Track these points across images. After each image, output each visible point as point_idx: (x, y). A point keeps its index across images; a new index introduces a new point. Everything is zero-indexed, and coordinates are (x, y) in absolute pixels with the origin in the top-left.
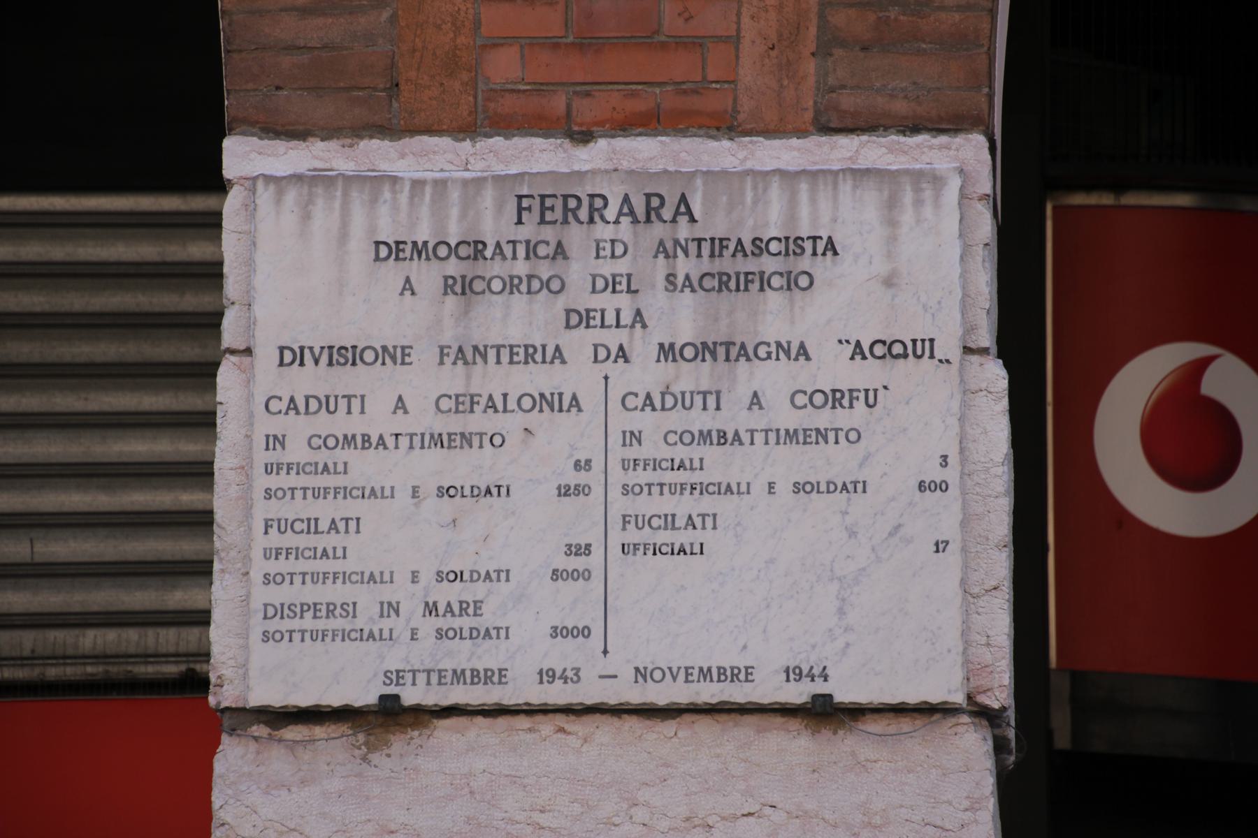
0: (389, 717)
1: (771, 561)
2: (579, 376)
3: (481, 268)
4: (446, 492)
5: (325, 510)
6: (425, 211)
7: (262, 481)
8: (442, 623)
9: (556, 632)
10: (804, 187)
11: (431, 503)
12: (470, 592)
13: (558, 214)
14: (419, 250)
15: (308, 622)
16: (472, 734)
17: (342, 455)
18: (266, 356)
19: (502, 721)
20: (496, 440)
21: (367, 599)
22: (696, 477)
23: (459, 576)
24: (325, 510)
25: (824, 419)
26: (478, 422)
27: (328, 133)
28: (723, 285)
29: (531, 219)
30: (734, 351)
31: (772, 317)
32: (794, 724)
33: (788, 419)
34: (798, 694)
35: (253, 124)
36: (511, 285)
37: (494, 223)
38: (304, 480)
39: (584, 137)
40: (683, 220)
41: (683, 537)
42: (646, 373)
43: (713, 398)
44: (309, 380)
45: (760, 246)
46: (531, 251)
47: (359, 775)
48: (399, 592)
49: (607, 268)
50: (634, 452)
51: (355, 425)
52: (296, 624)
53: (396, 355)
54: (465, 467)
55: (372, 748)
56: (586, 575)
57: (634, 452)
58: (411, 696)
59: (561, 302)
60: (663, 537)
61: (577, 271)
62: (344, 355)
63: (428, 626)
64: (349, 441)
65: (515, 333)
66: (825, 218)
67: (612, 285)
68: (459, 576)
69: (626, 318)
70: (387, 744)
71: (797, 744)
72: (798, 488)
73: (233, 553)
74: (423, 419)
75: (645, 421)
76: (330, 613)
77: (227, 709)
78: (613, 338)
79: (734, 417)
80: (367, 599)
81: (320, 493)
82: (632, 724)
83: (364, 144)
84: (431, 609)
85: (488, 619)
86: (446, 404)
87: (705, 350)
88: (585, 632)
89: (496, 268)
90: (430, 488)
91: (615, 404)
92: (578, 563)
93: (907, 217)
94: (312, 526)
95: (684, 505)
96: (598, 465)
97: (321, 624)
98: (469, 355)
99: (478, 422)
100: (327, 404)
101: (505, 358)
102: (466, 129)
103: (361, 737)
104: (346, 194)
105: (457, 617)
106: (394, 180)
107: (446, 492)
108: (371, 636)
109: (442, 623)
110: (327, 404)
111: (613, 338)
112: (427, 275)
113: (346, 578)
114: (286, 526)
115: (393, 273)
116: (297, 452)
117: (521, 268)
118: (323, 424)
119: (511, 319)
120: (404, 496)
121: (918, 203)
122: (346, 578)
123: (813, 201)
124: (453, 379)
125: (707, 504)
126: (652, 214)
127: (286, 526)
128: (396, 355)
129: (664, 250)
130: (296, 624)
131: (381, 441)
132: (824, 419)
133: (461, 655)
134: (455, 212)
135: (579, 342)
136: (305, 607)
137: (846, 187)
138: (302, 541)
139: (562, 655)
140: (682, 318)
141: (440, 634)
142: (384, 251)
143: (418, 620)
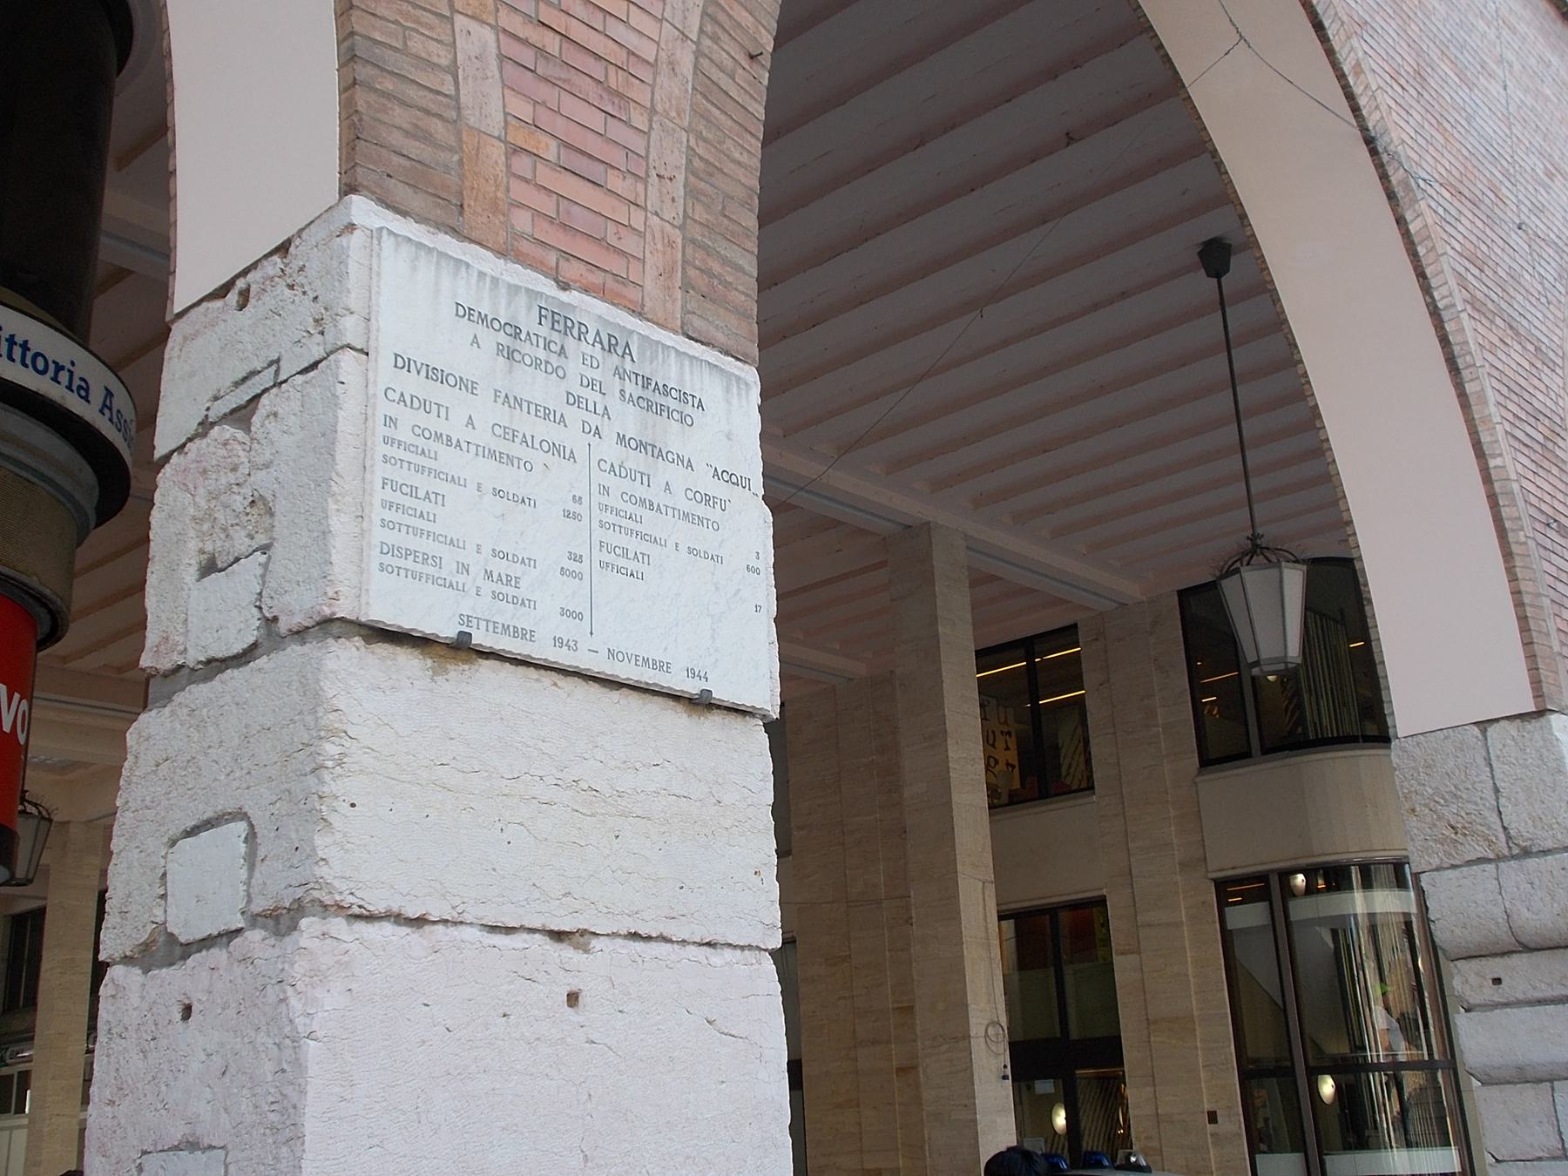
0: (462, 649)
1: (678, 595)
2: (571, 437)
3: (517, 345)
4: (497, 492)
5: (424, 483)
6: (486, 294)
7: (383, 449)
8: (499, 588)
9: (563, 612)
10: (687, 362)
11: (489, 498)
12: (517, 570)
13: (561, 328)
14: (483, 319)
15: (409, 563)
16: (503, 675)
17: (433, 445)
18: (384, 361)
19: (521, 669)
20: (528, 466)
21: (449, 556)
22: (638, 527)
23: (506, 556)
24: (424, 483)
25: (701, 510)
26: (516, 449)
27: (421, 220)
28: (649, 408)
29: (546, 323)
30: (656, 452)
31: (672, 436)
32: (679, 707)
33: (685, 506)
34: (692, 687)
35: (373, 193)
36: (536, 363)
37: (528, 322)
38: (407, 456)
39: (564, 286)
40: (628, 358)
41: (633, 566)
42: (609, 450)
43: (645, 478)
44: (413, 384)
45: (666, 391)
46: (547, 347)
47: (431, 690)
48: (468, 557)
49: (590, 374)
50: (605, 500)
51: (441, 426)
52: (401, 563)
53: (470, 387)
54: (509, 479)
55: (435, 673)
56: (579, 576)
57: (605, 500)
58: (480, 638)
59: (564, 386)
60: (621, 562)
61: (574, 367)
62: (436, 375)
63: (488, 587)
64: (439, 436)
65: (538, 397)
66: (688, 384)
67: (591, 384)
68: (506, 556)
69: (600, 410)
70: (446, 671)
71: (678, 719)
72: (690, 551)
73: (348, 499)
74: (482, 436)
75: (610, 480)
76: (425, 561)
77: (342, 619)
78: (594, 421)
79: (656, 495)
80: (449, 556)
81: (420, 469)
82: (595, 688)
83: (442, 236)
84: (489, 575)
85: (523, 593)
86: (498, 431)
87: (642, 446)
88: (580, 616)
89: (526, 348)
90: (488, 487)
91: (594, 464)
92: (574, 566)
93: (735, 401)
94: (413, 492)
95: (634, 545)
96: (585, 500)
97: (419, 568)
98: (512, 402)
99: (516, 449)
100: (424, 405)
101: (533, 411)
102: (501, 253)
103: (429, 662)
104: (438, 263)
105: (505, 586)
106: (468, 265)
107: (497, 492)
108: (451, 585)
109: (499, 588)
110: (424, 405)
111: (594, 421)
112: (489, 339)
113: (436, 537)
114: (398, 487)
115: (467, 329)
116: (404, 434)
117: (542, 354)
118: (421, 418)
119: (536, 387)
120: (472, 487)
121: (739, 394)
122: (436, 537)
123: (692, 373)
124: (502, 415)
125: (644, 547)
126: (611, 348)
127: (398, 487)
128: (470, 387)
129: (620, 373)
130: (401, 563)
131: (458, 444)
132: (701, 510)
133: (507, 614)
134: (503, 302)
135: (574, 415)
136: (408, 552)
137: (706, 370)
138: (408, 502)
139: (567, 628)
140: (629, 420)
141: (495, 596)
142: (461, 312)
143: (480, 582)
